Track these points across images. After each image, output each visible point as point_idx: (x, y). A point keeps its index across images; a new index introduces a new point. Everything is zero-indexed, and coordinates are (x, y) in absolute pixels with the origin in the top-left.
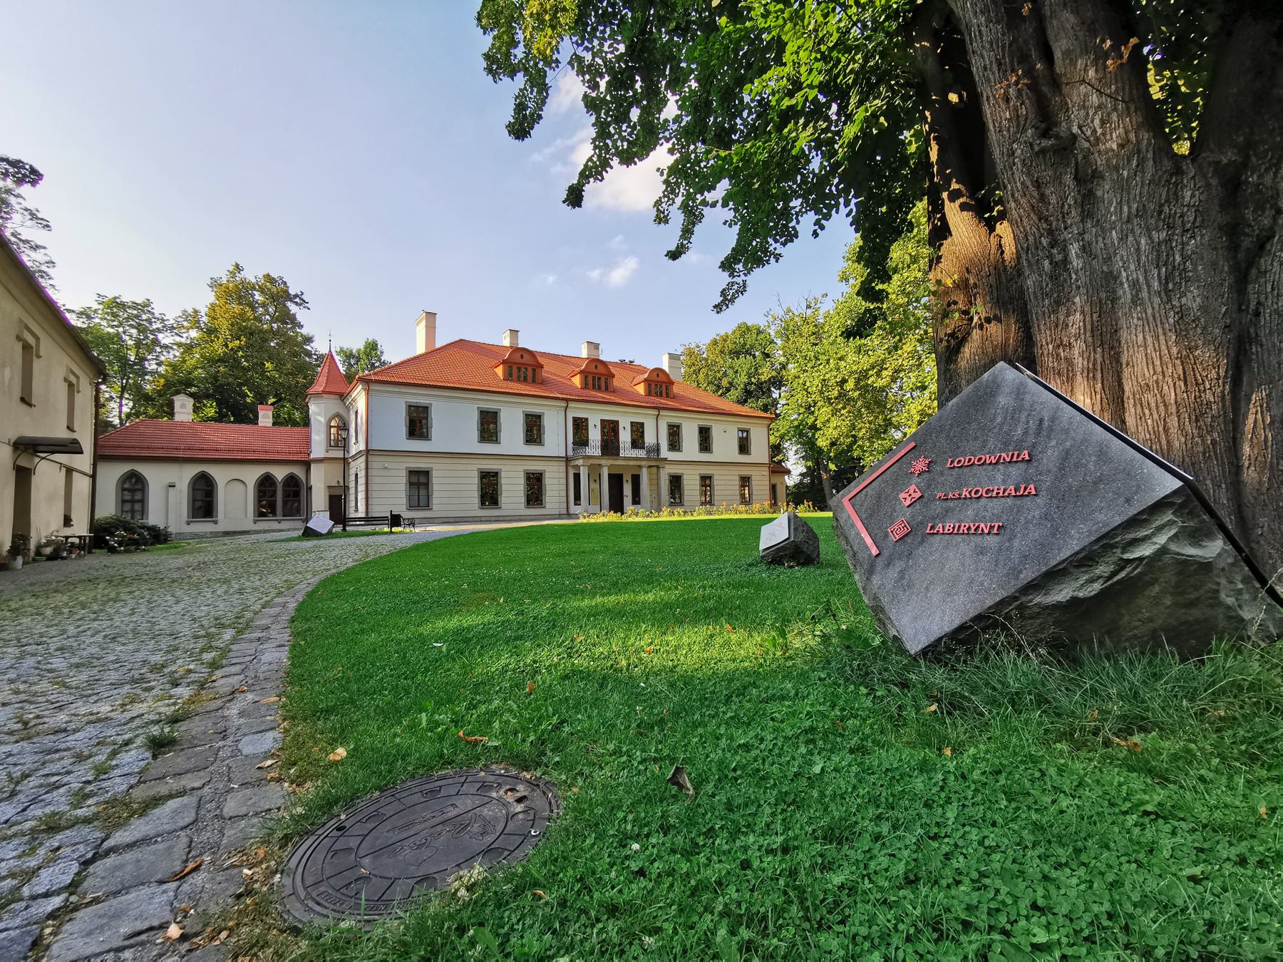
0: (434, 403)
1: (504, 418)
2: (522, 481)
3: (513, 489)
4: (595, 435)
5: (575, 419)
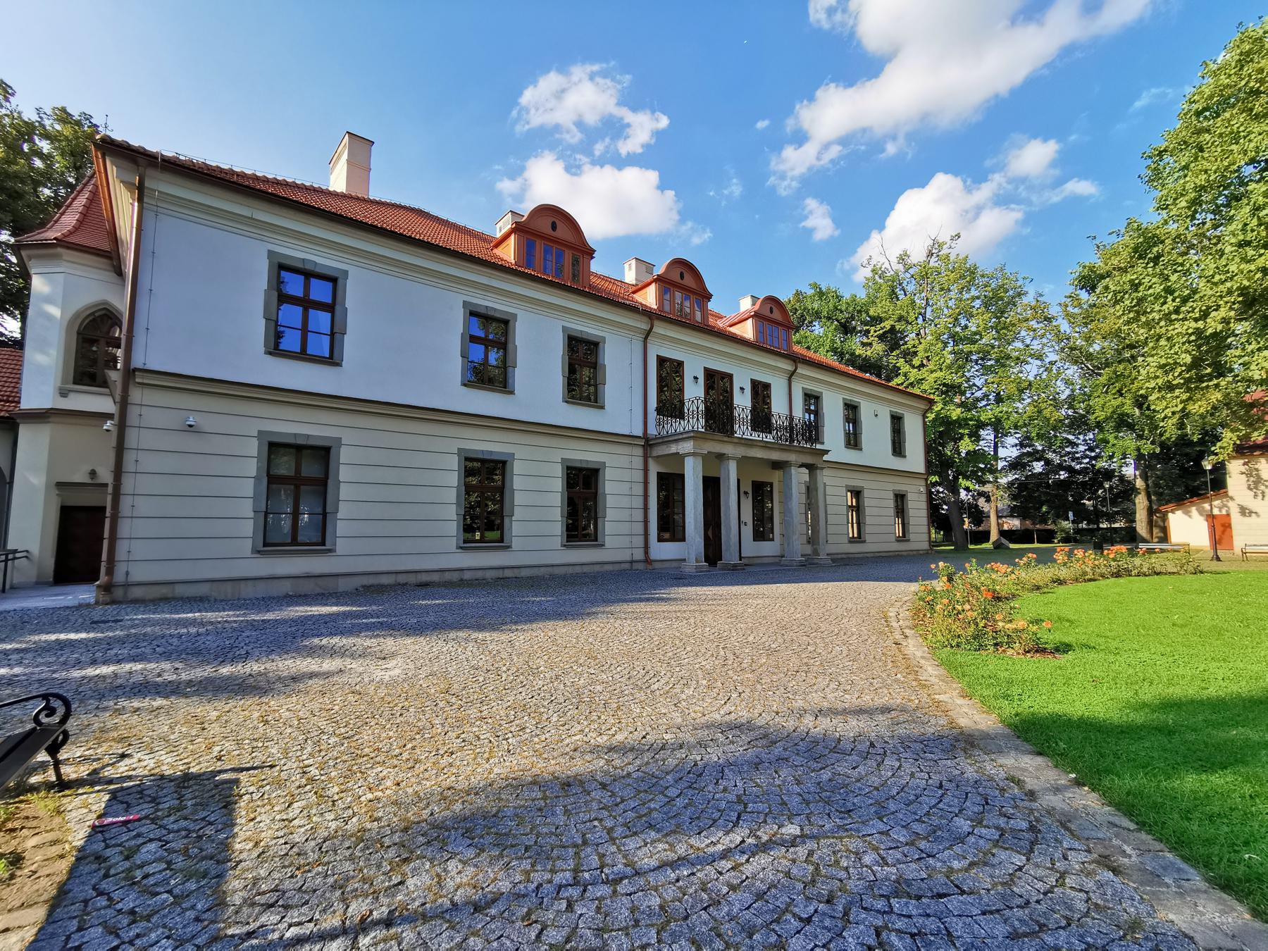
0: (353, 272)
1: (522, 335)
2: (558, 485)
3: (536, 498)
4: (694, 392)
5: (661, 361)
